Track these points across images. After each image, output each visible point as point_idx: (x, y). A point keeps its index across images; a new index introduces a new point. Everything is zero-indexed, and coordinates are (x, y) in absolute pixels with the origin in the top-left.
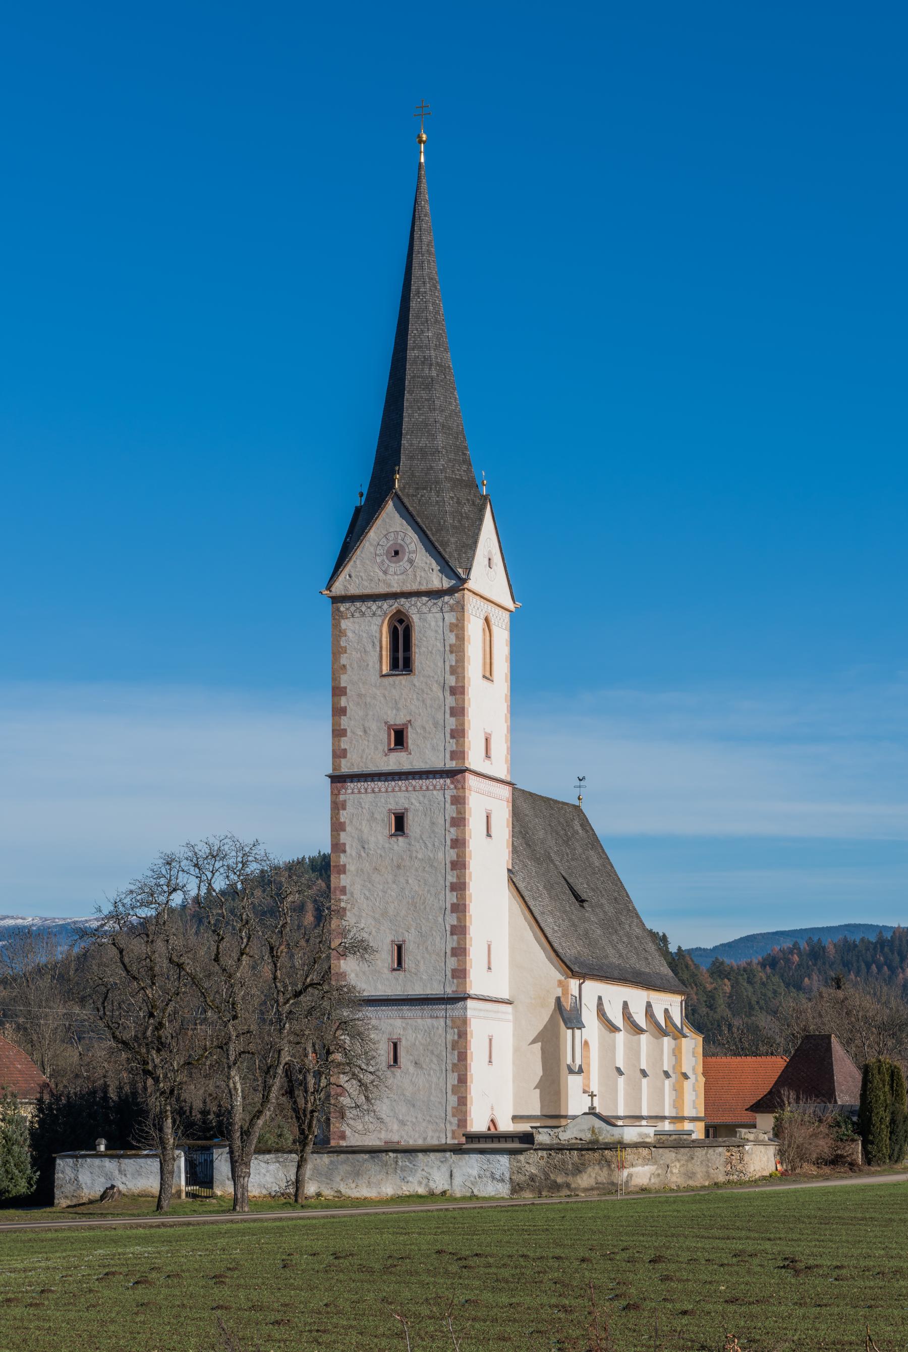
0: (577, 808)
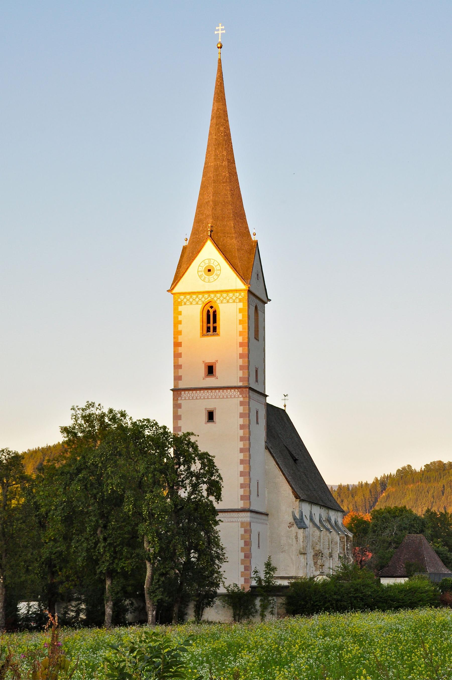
0: (284, 411)
